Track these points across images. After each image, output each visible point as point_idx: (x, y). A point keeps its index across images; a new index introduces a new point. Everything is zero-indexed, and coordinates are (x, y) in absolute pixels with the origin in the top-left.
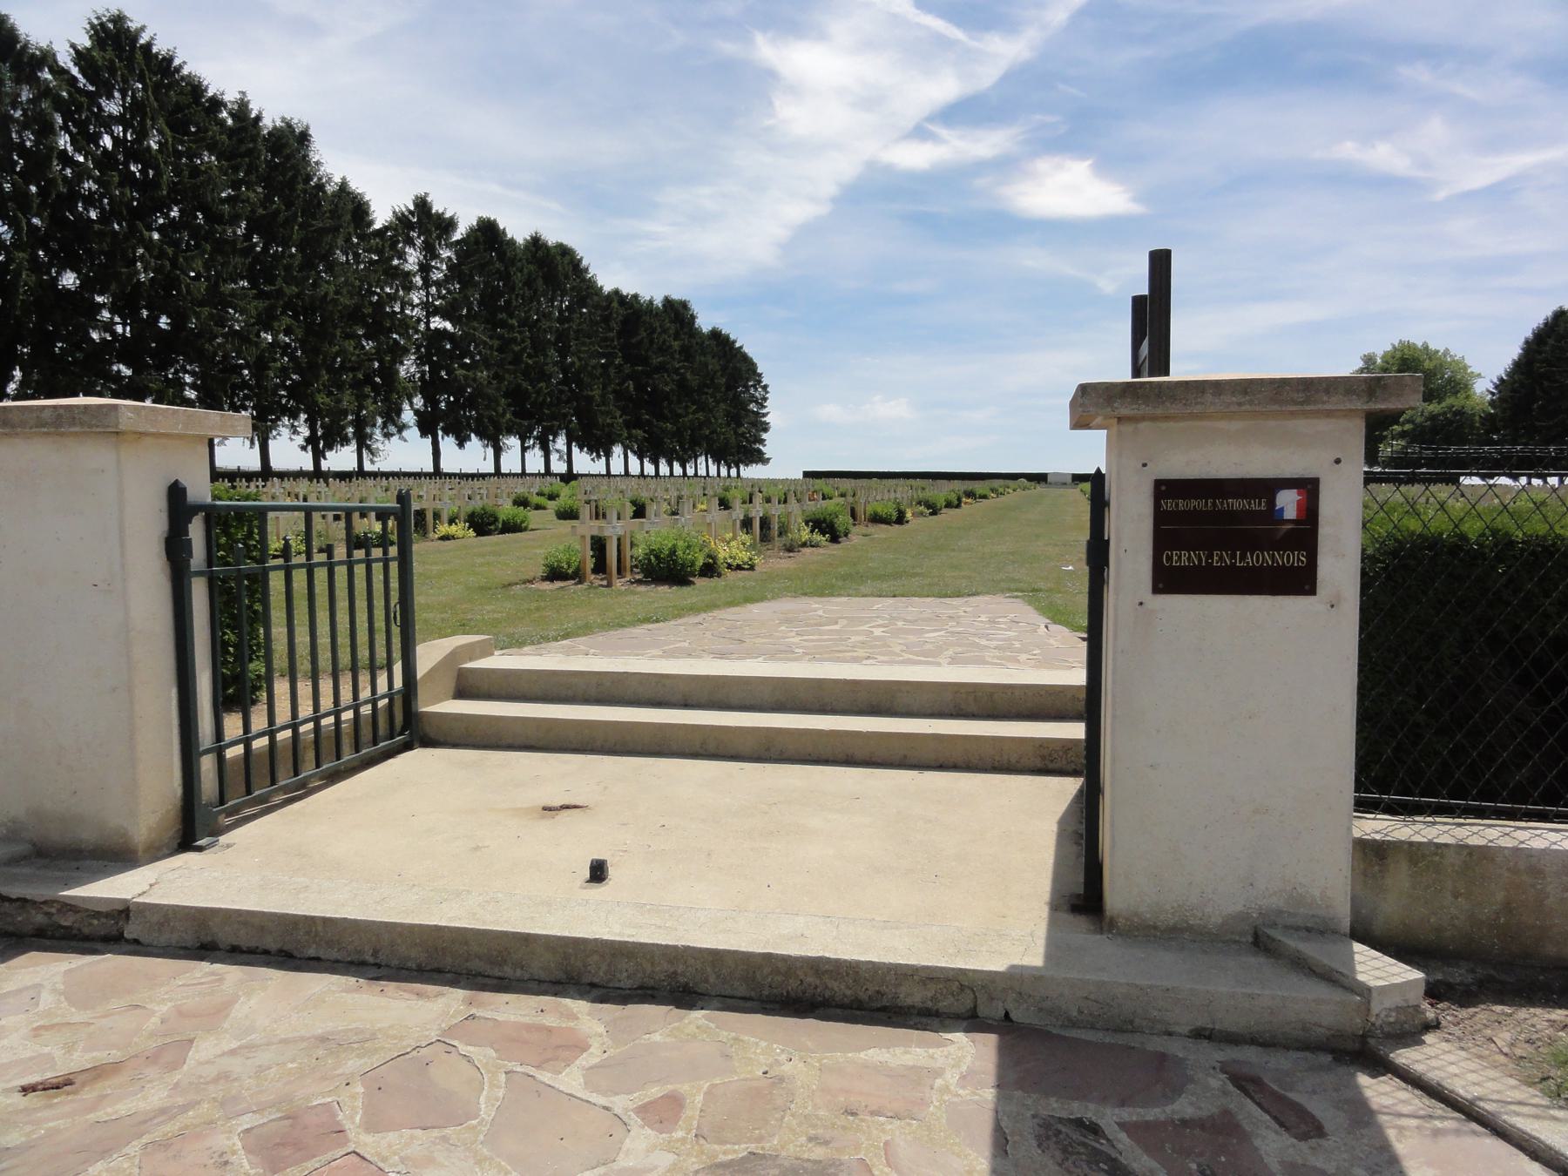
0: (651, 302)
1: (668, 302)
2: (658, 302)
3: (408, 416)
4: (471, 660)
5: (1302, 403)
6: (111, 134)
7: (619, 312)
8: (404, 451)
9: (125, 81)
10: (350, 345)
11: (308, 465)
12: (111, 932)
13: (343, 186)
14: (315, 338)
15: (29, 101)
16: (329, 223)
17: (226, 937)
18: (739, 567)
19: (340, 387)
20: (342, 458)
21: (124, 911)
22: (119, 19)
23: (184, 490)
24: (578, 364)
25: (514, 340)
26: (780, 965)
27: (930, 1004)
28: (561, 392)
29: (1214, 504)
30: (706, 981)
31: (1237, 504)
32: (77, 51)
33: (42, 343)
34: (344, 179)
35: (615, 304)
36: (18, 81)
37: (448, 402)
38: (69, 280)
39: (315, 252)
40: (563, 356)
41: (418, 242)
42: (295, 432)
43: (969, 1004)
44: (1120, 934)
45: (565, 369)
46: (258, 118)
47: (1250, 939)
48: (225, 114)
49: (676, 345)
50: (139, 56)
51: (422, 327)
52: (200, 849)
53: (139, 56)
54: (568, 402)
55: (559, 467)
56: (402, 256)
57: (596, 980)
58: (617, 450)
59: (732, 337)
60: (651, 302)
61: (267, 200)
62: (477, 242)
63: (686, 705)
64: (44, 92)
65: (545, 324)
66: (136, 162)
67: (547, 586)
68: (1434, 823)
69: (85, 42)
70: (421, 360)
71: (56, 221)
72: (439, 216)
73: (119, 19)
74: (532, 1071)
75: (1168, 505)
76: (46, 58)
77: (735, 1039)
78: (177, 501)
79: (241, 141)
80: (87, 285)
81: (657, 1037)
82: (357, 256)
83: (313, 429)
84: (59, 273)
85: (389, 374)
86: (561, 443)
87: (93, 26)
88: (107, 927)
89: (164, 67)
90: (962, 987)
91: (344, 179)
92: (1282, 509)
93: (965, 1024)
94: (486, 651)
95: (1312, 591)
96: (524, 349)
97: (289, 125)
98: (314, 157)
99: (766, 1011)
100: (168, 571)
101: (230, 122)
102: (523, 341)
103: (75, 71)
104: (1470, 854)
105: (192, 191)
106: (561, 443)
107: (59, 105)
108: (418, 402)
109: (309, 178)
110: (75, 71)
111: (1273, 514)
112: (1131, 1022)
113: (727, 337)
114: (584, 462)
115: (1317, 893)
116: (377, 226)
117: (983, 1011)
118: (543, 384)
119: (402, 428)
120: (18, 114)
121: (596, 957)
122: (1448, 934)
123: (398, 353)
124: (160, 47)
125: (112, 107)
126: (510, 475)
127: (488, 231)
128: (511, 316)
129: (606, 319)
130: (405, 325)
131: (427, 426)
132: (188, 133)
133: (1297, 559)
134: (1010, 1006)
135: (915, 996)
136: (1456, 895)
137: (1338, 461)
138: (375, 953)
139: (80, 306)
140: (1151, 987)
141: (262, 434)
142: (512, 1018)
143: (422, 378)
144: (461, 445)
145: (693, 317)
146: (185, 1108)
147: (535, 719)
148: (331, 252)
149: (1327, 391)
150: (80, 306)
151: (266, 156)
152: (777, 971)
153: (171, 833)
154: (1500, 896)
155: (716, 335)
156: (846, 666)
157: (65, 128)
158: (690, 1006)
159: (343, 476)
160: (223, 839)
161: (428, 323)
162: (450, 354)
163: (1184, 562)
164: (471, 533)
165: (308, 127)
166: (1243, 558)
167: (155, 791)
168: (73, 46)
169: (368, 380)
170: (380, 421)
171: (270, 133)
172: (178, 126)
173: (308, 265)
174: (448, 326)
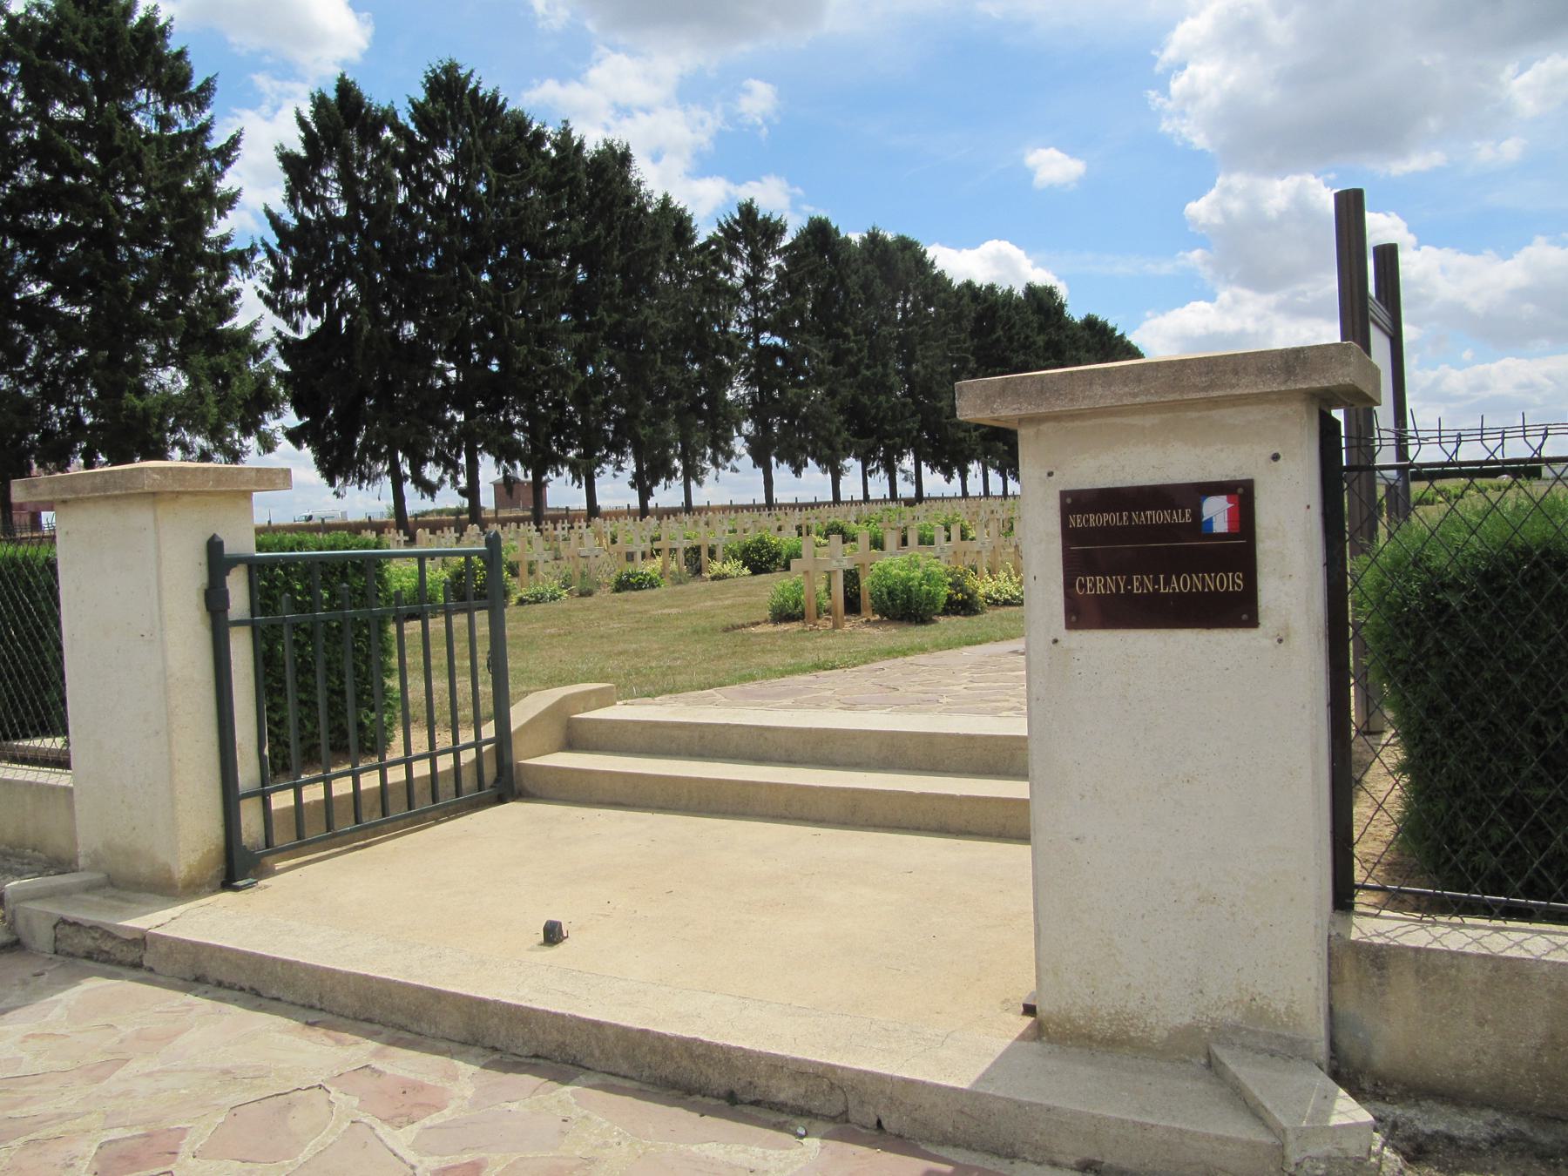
0: (1010, 291)
1: (1031, 290)
2: (1019, 291)
3: (739, 445)
4: (586, 710)
5: (1204, 389)
6: (444, 182)
7: (972, 311)
8: (731, 482)
9: (455, 129)
10: (672, 372)
11: (635, 503)
12: (133, 958)
13: (666, 201)
14: (635, 369)
15: (373, 160)
16: (650, 244)
17: (216, 971)
18: (1007, 603)
19: (664, 416)
20: (667, 495)
21: (142, 941)
22: (451, 69)
23: (221, 544)
24: (922, 372)
25: (850, 351)
26: (657, 1044)
27: (802, 1102)
28: (905, 405)
29: (1130, 518)
30: (592, 1055)
31: (1156, 517)
32: (414, 106)
33: (385, 392)
34: (666, 195)
35: (966, 300)
36: (363, 144)
37: (781, 425)
38: (410, 329)
39: (638, 281)
40: (908, 363)
41: (745, 254)
42: (620, 469)
43: (841, 1108)
44: (1050, 1041)
45: (908, 377)
46: (580, 146)
47: (1203, 1061)
48: (548, 145)
49: (1040, 340)
50: (466, 101)
51: (750, 345)
52: (237, 889)
53: (466, 101)
54: (913, 415)
55: (906, 490)
56: (729, 270)
57: (498, 1045)
58: (974, 468)
59: (1111, 324)
60: (1010, 291)
61: (589, 227)
62: (807, 245)
63: (790, 760)
64: (386, 150)
65: (885, 330)
66: (467, 206)
67: (769, 628)
68: (1463, 925)
69: (421, 96)
70: (750, 381)
71: (396, 275)
72: (766, 220)
73: (451, 69)
74: (376, 1123)
75: (1077, 521)
76: (389, 118)
77: (586, 1117)
78: (217, 560)
79: (564, 171)
80: (424, 332)
81: (514, 1106)
82: (681, 276)
83: (639, 466)
84: (400, 325)
85: (715, 398)
86: (908, 463)
87: (429, 79)
88: (132, 955)
89: (491, 108)
90: (832, 1086)
91: (666, 195)
92: (1210, 521)
93: (831, 1127)
94: (604, 699)
95: (1253, 622)
96: (860, 361)
97: (610, 147)
98: (634, 177)
99: (640, 1094)
100: (208, 621)
101: (553, 153)
102: (860, 350)
103: (412, 126)
104: (1497, 969)
105: (515, 231)
106: (908, 463)
107: (398, 161)
108: (748, 427)
109: (629, 200)
110: (412, 126)
111: (1199, 526)
112: (1012, 1145)
113: (1105, 325)
114: (934, 482)
115: (1282, 1007)
116: (701, 240)
117: (854, 1115)
118: (882, 398)
119: (729, 455)
120: (364, 175)
121: (496, 1020)
122: (1471, 1073)
123: (722, 377)
124: (486, 89)
125: (445, 156)
126: (852, 502)
127: (819, 233)
128: (846, 324)
129: (958, 318)
130: (731, 346)
131: (760, 457)
132: (515, 171)
133: (1233, 582)
134: (883, 1113)
135: (786, 1092)
136: (1481, 1022)
137: (1276, 457)
138: (321, 998)
139: (416, 356)
140: (1031, 1104)
141: (585, 473)
142: (400, 1073)
143: (753, 399)
144: (797, 472)
145: (1062, 306)
146: (83, 1114)
147: (845, 790)
148: (653, 274)
149: (1236, 373)
150: (416, 356)
151: (586, 181)
152: (653, 1050)
153: (212, 873)
154: (1541, 1028)
155: (1091, 323)
156: (974, 719)
157: (404, 182)
158: (563, 1079)
159: (671, 512)
160: (262, 883)
161: (757, 340)
162: (781, 373)
163: (1100, 590)
164: (746, 571)
165: (628, 147)
166: (1167, 582)
167: (194, 834)
168: (411, 101)
169: (695, 408)
170: (709, 451)
171: (593, 160)
172: (504, 164)
173: (630, 291)
174: (779, 340)
